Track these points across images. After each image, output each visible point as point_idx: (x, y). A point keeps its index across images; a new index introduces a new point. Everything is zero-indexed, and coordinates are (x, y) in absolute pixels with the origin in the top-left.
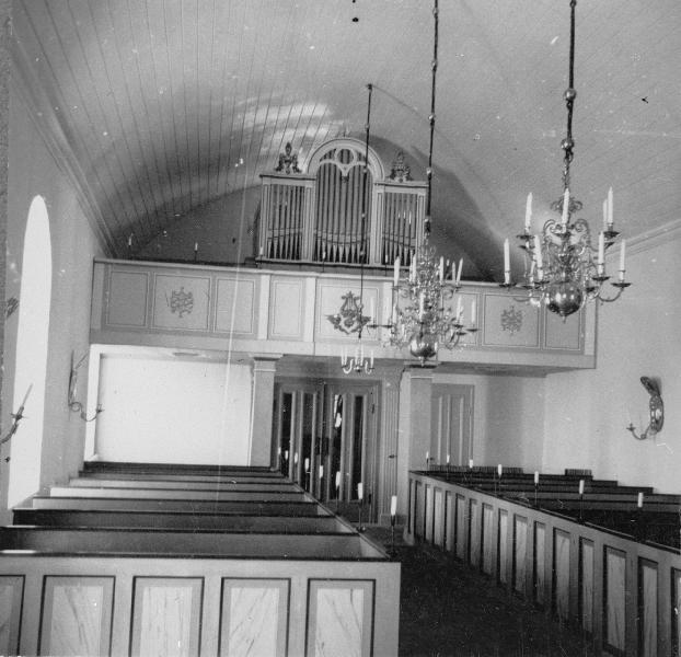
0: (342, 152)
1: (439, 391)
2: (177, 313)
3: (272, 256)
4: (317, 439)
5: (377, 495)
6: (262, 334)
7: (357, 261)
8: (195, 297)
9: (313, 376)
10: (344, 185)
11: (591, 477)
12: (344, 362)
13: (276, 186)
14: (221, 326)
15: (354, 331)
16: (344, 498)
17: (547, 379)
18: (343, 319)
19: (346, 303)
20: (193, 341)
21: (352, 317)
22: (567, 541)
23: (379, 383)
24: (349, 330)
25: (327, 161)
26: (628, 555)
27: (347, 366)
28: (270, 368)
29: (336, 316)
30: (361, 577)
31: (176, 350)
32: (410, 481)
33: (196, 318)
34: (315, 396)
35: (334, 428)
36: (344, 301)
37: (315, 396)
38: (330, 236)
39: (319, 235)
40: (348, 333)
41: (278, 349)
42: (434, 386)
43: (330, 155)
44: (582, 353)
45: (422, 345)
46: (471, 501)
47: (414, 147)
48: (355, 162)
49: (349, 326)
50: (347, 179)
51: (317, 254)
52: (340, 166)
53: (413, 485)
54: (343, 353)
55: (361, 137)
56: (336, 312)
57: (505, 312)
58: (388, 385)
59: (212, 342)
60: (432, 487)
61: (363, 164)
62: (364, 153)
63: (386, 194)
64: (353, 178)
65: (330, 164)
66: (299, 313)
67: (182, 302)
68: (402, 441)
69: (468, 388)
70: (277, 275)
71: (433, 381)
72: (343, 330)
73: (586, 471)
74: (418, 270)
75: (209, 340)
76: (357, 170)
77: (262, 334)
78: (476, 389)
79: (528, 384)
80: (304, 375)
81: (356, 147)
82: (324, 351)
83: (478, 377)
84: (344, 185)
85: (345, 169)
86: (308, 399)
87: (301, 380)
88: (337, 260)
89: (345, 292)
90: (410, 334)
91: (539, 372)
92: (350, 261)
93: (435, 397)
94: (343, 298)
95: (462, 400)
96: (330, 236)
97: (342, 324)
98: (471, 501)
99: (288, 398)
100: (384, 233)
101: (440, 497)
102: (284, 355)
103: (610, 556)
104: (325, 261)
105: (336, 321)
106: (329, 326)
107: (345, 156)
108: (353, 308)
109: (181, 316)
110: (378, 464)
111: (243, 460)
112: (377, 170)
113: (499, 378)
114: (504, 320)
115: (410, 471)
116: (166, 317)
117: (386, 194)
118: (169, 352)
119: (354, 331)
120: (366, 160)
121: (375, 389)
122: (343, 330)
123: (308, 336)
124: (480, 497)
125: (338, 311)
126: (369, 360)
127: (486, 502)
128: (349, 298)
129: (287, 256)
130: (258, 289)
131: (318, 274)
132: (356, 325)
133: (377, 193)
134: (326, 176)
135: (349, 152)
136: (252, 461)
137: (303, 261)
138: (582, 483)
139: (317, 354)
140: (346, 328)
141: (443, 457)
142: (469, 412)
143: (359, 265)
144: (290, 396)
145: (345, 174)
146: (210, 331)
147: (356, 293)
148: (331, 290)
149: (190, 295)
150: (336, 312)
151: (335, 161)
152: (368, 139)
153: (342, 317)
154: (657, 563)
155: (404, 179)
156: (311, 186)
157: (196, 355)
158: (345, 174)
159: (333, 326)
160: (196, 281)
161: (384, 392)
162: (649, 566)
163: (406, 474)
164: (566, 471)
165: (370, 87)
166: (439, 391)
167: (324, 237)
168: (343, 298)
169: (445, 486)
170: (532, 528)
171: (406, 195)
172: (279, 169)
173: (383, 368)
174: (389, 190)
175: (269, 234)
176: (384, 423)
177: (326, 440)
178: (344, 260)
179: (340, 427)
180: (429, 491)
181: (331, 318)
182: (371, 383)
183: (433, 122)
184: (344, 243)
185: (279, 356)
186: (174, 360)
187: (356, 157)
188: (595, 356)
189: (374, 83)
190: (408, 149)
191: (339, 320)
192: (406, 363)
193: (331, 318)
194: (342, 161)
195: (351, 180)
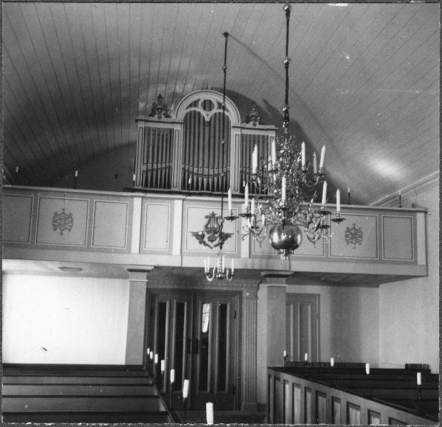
0: (205, 101)
1: (292, 299)
2: (58, 230)
3: (146, 186)
4: (188, 340)
5: (240, 389)
6: (135, 247)
7: (218, 189)
8: (74, 216)
9: (183, 287)
10: (207, 129)
11: (430, 370)
12: (207, 271)
13: (149, 129)
14: (98, 242)
15: (216, 246)
16: (212, 389)
17: (379, 288)
18: (207, 236)
19: (209, 222)
20: (72, 255)
21: (215, 234)
22: (299, 390)
23: (240, 293)
24: (212, 245)
25: (193, 109)
26: (382, 415)
27: (210, 274)
28: (143, 279)
29: (200, 233)
30: (228, 50)
31: (60, 265)
32: (269, 376)
33: (76, 235)
34: (186, 304)
35: (202, 333)
36: (207, 220)
37: (186, 304)
38: (196, 169)
39: (187, 169)
40: (211, 248)
41: (150, 261)
42: (288, 295)
43: (195, 104)
44: (415, 263)
45: (284, 237)
46: (334, 399)
47: (265, 101)
48: (216, 110)
49: (212, 241)
50: (209, 123)
51: (184, 185)
52: (203, 113)
53: (272, 380)
54: (207, 263)
55: (220, 91)
56: (200, 229)
57: (348, 228)
58: (248, 294)
59: (92, 257)
60: (291, 383)
61: (221, 111)
62: (221, 101)
63: (242, 135)
64: (215, 121)
65: (195, 111)
66: (166, 232)
67: (62, 221)
68: (261, 339)
69: (315, 297)
70: (148, 198)
71: (287, 291)
72: (207, 245)
73: (424, 365)
74: (278, 158)
75: (84, 254)
76: (217, 116)
77: (135, 247)
78: (321, 296)
79: (364, 292)
80: (175, 287)
81: (216, 98)
82: (190, 262)
83: (325, 287)
84: (207, 129)
85: (207, 115)
86: (172, 300)
87: (173, 291)
88: (202, 189)
89: (208, 212)
90: (270, 227)
91: (374, 281)
92: (213, 190)
93: (288, 304)
94: (206, 217)
95: (309, 307)
96: (196, 169)
97: (206, 239)
98: (334, 399)
99: (162, 306)
100: (242, 166)
101: (298, 392)
102: (156, 267)
103: (351, 409)
104: (191, 189)
105: (200, 238)
106: (194, 243)
107: (208, 105)
108: (216, 226)
109: (61, 234)
110: (240, 361)
111: (120, 360)
112: (233, 115)
113: (344, 289)
114: (347, 236)
115: (269, 368)
116: (48, 234)
117: (242, 135)
118: (55, 266)
119: (216, 246)
120: (224, 108)
121: (237, 298)
122: (207, 245)
123: (176, 250)
124: (344, 396)
125: (202, 229)
126: (230, 270)
127: (350, 400)
128: (212, 217)
129: (158, 184)
130: (131, 210)
131: (184, 197)
132: (217, 242)
133: (235, 133)
134: (192, 121)
135: (210, 102)
136: (127, 360)
137: (173, 189)
138: (419, 375)
139: (183, 266)
140: (210, 243)
141: (302, 356)
142: (316, 317)
143: (220, 193)
144: (165, 305)
145: (207, 119)
146: (88, 247)
147: (218, 213)
148: (198, 212)
149: (70, 216)
150: (200, 229)
151: (199, 109)
152: (224, 92)
153: (206, 234)
154: (379, 414)
155: (257, 123)
156: (179, 129)
157: (81, 269)
158: (207, 119)
159: (197, 241)
160: (74, 204)
161: (244, 301)
162: (353, 408)
163: (266, 370)
164: (407, 365)
165: (226, 35)
166: (292, 299)
167: (191, 170)
168: (206, 217)
169: (303, 382)
170: (345, 407)
171: (259, 136)
172: (152, 115)
173: (243, 281)
174: (245, 132)
175: (144, 168)
176: (244, 327)
177: (195, 341)
178: (208, 189)
179: (208, 332)
180: (288, 387)
181: (196, 235)
182: (235, 293)
183: (287, 64)
184: (206, 171)
185: (150, 268)
186: (60, 275)
187: (216, 106)
188: (427, 265)
189: (229, 32)
190: (259, 102)
191: (203, 236)
192: (263, 273)
193: (196, 235)
194: (205, 109)
195: (212, 125)
